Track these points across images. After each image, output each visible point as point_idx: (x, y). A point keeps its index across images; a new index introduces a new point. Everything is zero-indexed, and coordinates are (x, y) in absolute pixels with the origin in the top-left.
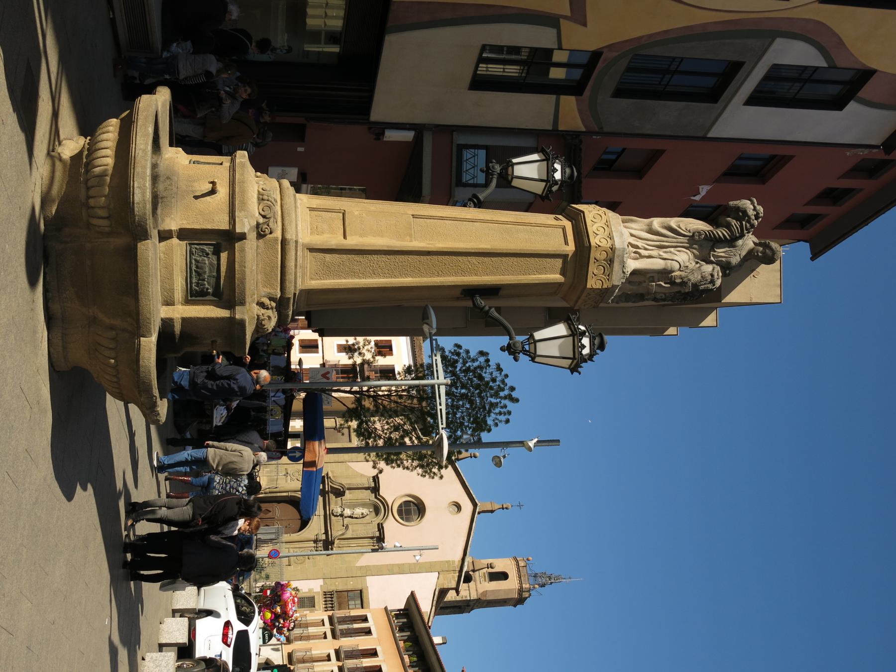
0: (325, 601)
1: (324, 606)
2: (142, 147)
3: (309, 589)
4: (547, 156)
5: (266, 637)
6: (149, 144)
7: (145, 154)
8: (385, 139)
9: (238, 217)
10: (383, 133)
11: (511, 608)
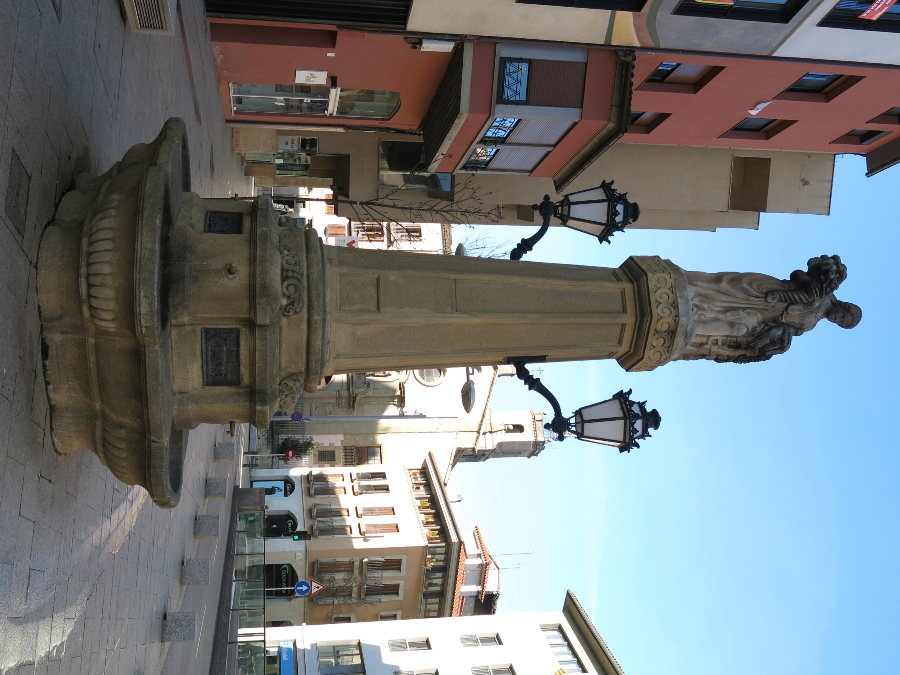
0: (346, 456)
1: (344, 454)
2: (149, 246)
3: (330, 443)
4: (609, 196)
5: (290, 526)
6: (157, 241)
7: (152, 255)
8: (422, 50)
9: (260, 304)
10: (421, 44)
11: (526, 459)
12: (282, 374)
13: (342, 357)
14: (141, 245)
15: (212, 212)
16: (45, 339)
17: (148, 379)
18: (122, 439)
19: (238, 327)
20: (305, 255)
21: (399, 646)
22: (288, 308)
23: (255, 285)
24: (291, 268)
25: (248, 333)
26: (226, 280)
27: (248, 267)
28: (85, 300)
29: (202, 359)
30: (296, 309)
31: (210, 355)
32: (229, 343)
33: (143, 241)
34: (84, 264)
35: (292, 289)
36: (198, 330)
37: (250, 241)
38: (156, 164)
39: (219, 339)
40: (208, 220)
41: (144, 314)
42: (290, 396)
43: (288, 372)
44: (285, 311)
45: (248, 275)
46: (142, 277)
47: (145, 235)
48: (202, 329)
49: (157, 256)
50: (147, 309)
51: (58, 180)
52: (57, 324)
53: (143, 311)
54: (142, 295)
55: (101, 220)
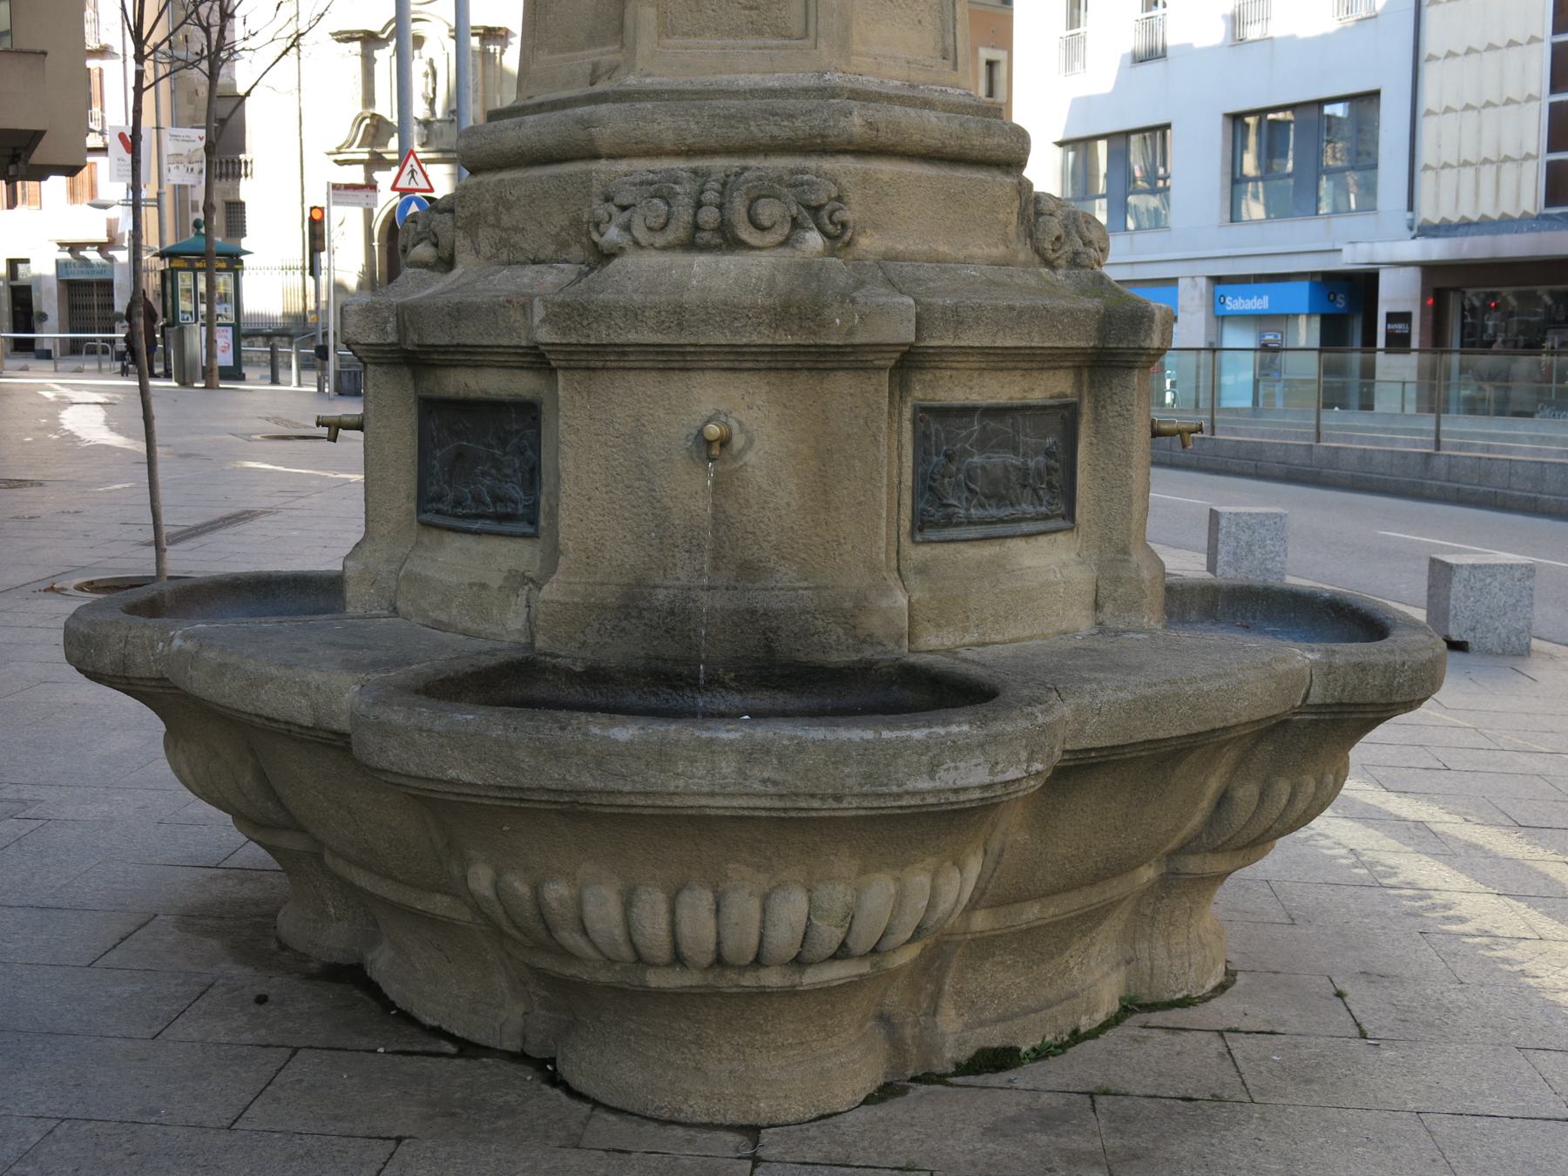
2: (728, 766)
6: (705, 735)
7: (768, 752)
9: (851, 332)
12: (1022, 257)
13: (950, 40)
14: (725, 795)
15: (421, 509)
16: (958, 1065)
17: (1161, 735)
18: (1263, 795)
19: (907, 413)
20: (603, 165)
21: (1073, 50)
22: (830, 228)
23: (775, 351)
24: (684, 215)
25: (929, 376)
26: (750, 457)
27: (697, 378)
28: (873, 966)
29: (1006, 537)
30: (830, 199)
31: (993, 512)
32: (959, 446)
33: (706, 789)
34: (748, 980)
35: (768, 211)
36: (918, 554)
37: (588, 369)
38: (343, 735)
39: (946, 480)
40: (477, 525)
41: (992, 773)
42: (1087, 234)
43: (1018, 236)
44: (839, 237)
45: (729, 375)
46: (856, 790)
47: (681, 783)
48: (914, 541)
49: (770, 734)
50: (974, 761)
51: (375, 1051)
52: (908, 1032)
53: (980, 776)
54: (924, 784)
55: (584, 932)
